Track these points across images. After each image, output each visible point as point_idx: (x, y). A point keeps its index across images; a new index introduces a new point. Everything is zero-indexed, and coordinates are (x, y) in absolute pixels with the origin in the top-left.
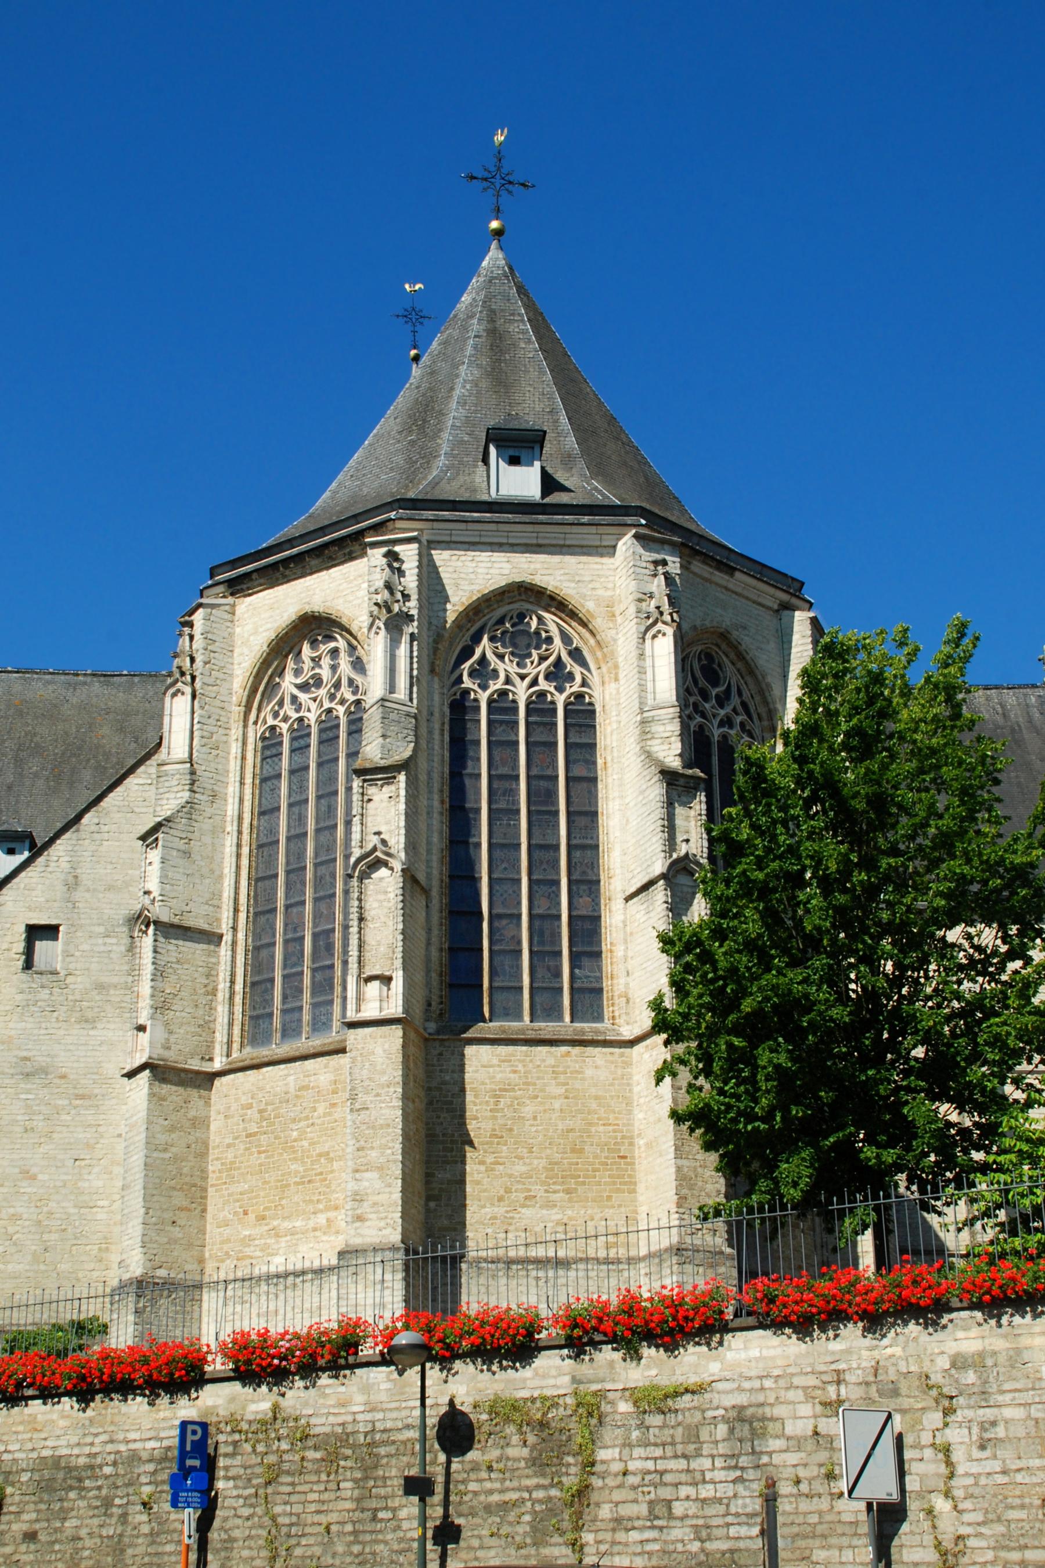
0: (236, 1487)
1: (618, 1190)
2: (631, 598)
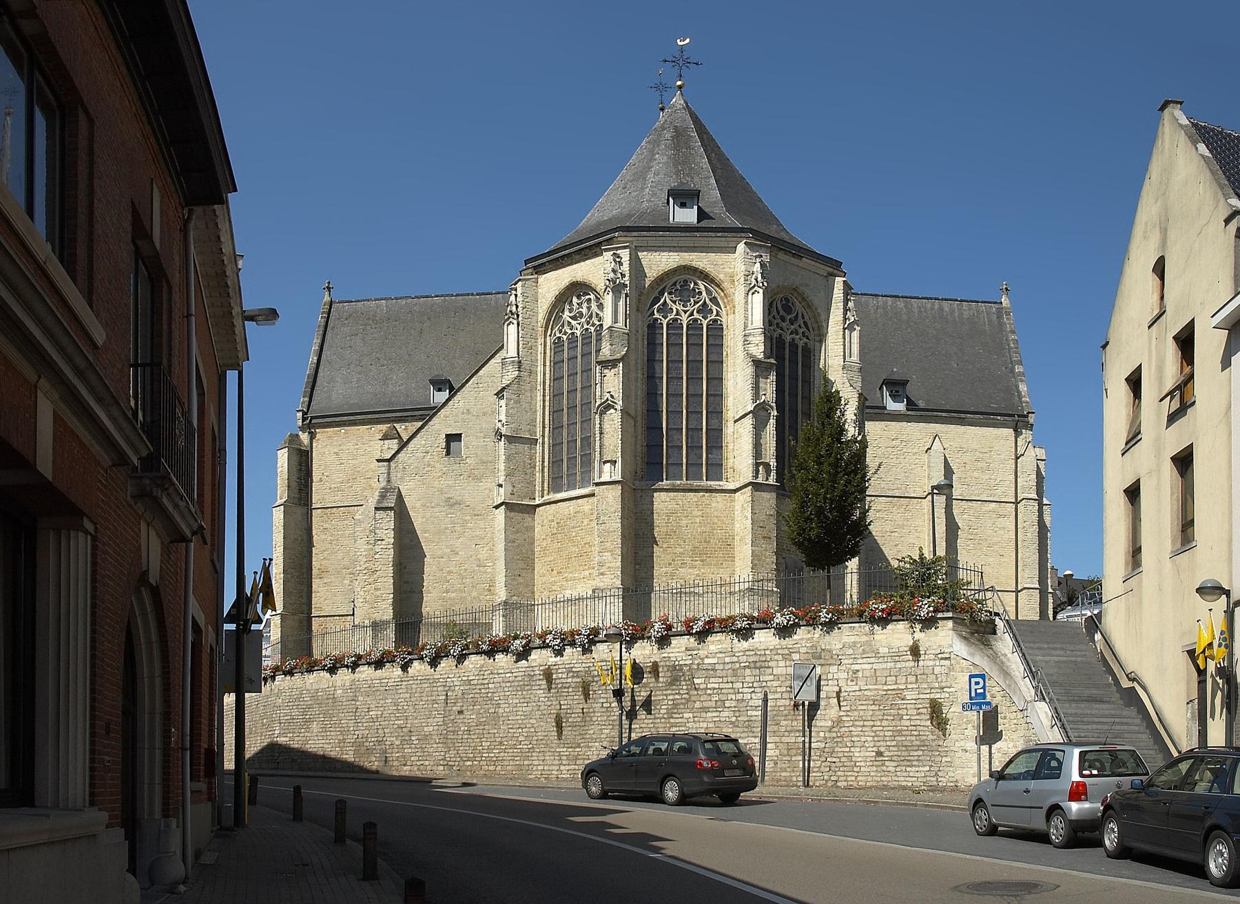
0: (544, 693)
1: (726, 560)
2: (742, 274)
